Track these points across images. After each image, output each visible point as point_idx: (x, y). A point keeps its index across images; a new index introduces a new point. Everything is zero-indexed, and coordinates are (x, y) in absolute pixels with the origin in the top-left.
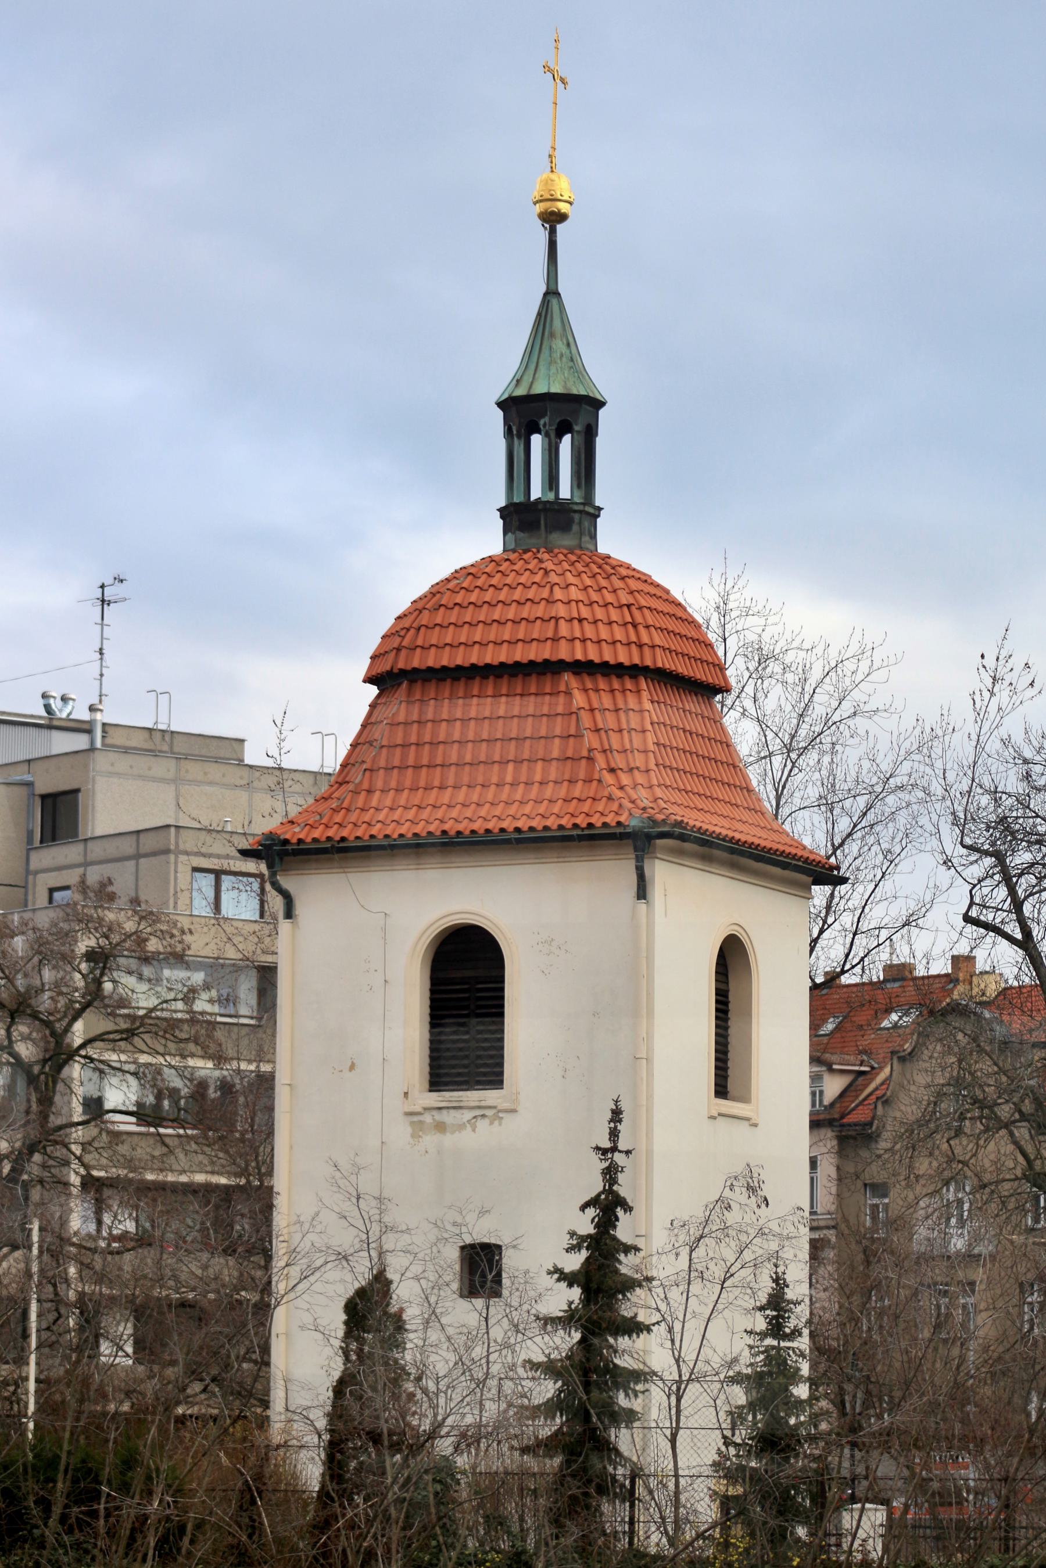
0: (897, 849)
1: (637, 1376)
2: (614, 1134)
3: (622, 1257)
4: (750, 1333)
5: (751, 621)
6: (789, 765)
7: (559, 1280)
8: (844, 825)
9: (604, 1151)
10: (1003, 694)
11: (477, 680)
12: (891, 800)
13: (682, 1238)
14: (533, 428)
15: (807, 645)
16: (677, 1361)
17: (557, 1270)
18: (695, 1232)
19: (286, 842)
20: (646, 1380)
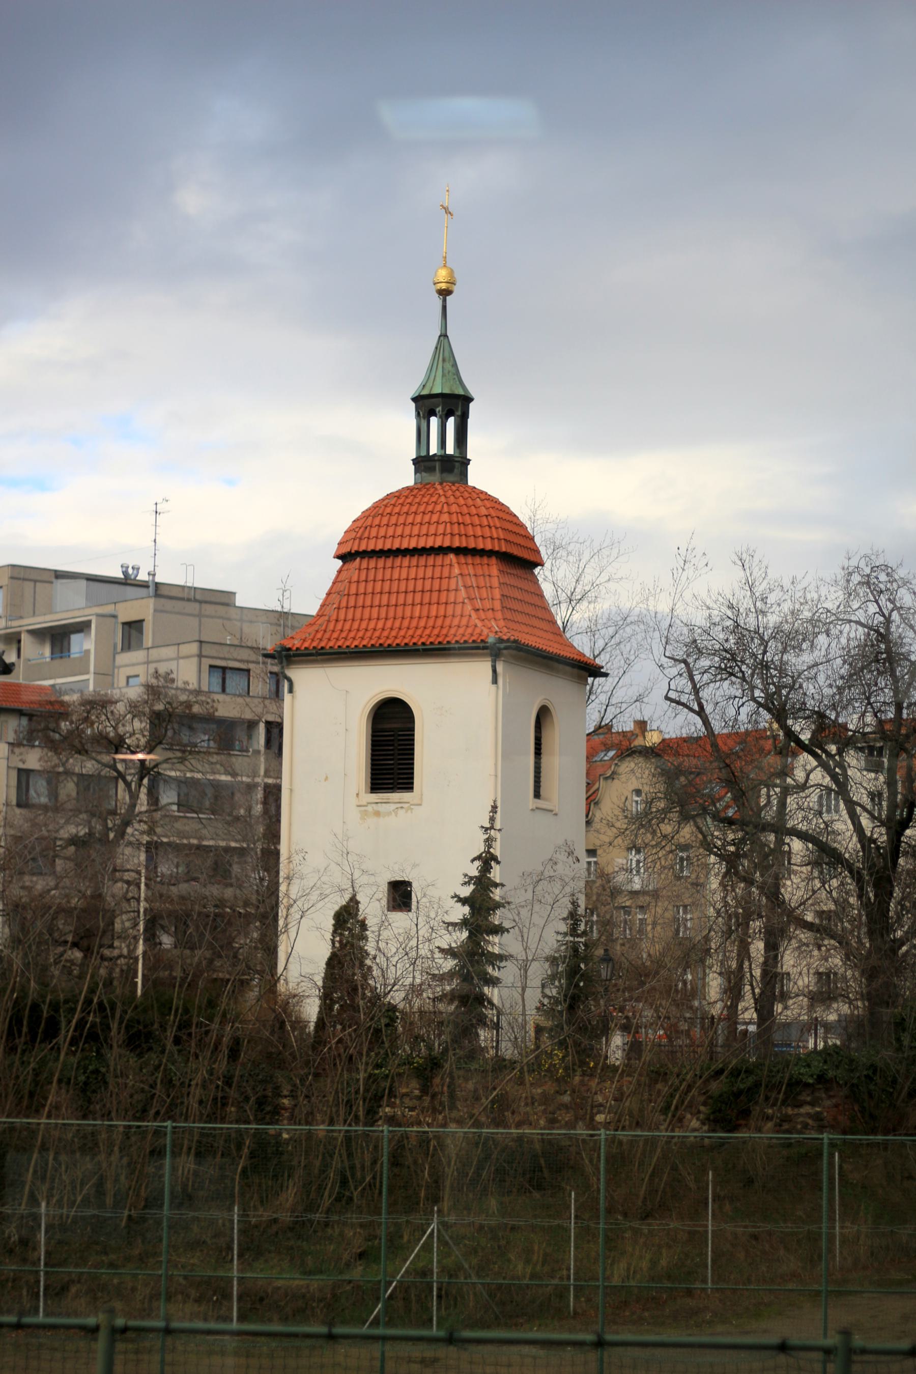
0: (632, 658)
1: (501, 958)
2: (492, 819)
3: (493, 889)
4: (558, 933)
5: (549, 526)
6: (571, 609)
7: (457, 901)
8: (600, 644)
9: (487, 829)
10: (690, 571)
11: (416, 557)
12: (628, 629)
13: (528, 881)
14: (432, 413)
15: (581, 540)
16: (525, 950)
17: (456, 896)
18: (535, 878)
19: (289, 649)
20: (506, 960)
